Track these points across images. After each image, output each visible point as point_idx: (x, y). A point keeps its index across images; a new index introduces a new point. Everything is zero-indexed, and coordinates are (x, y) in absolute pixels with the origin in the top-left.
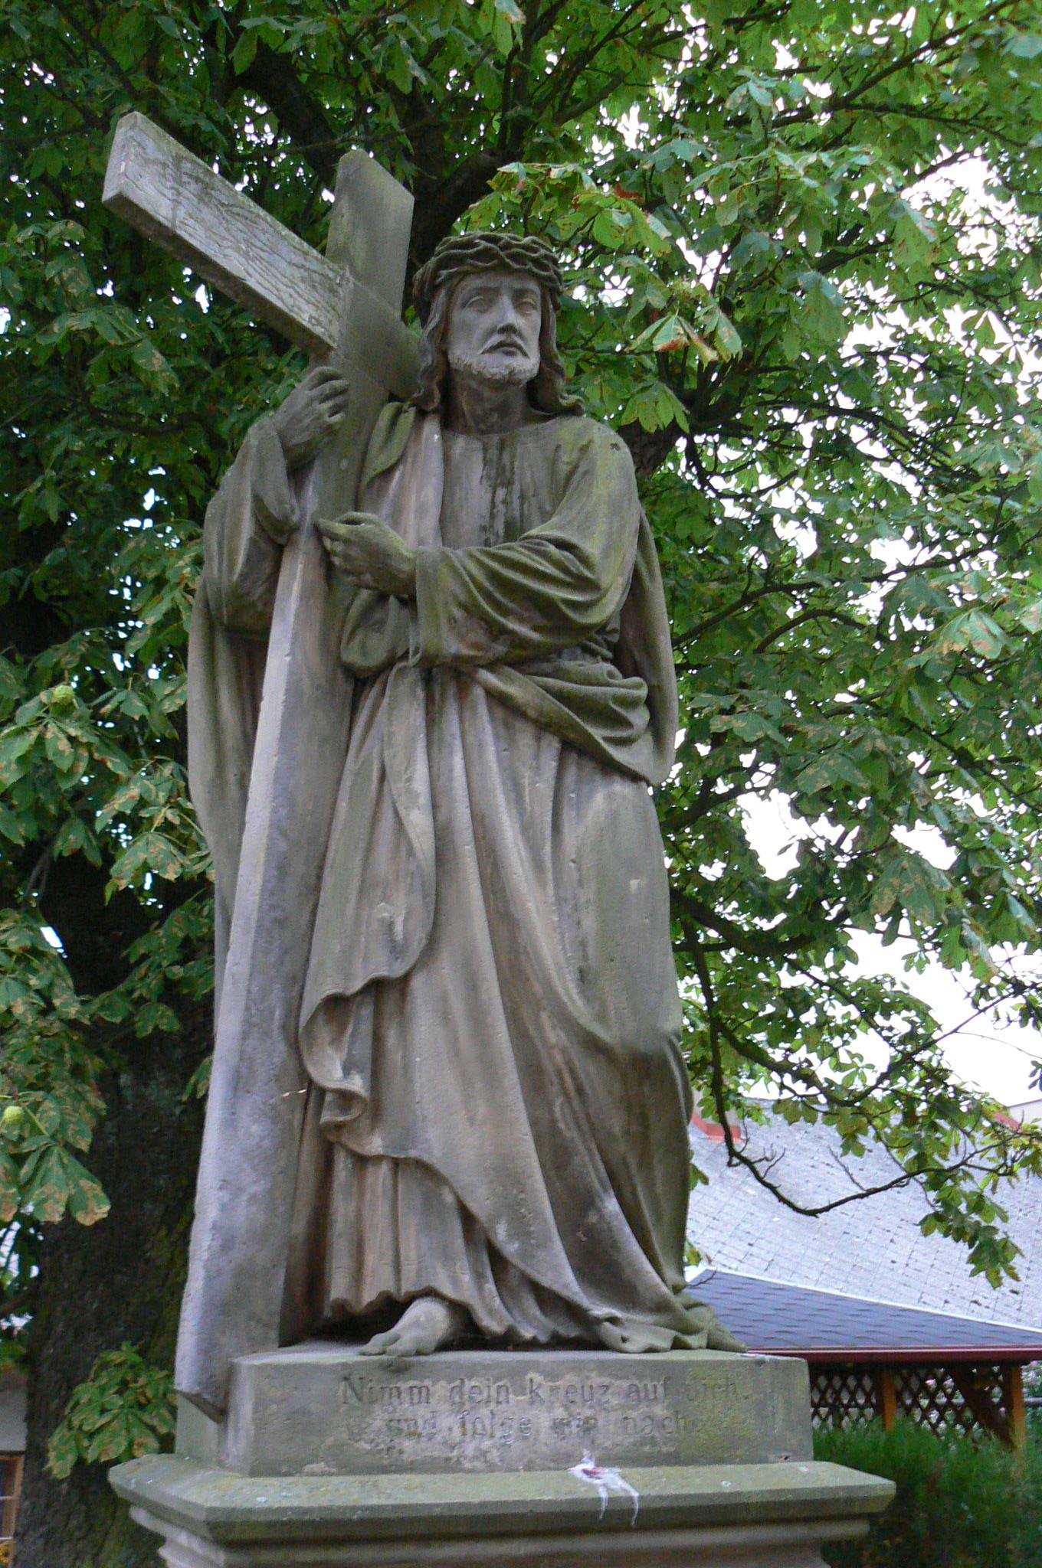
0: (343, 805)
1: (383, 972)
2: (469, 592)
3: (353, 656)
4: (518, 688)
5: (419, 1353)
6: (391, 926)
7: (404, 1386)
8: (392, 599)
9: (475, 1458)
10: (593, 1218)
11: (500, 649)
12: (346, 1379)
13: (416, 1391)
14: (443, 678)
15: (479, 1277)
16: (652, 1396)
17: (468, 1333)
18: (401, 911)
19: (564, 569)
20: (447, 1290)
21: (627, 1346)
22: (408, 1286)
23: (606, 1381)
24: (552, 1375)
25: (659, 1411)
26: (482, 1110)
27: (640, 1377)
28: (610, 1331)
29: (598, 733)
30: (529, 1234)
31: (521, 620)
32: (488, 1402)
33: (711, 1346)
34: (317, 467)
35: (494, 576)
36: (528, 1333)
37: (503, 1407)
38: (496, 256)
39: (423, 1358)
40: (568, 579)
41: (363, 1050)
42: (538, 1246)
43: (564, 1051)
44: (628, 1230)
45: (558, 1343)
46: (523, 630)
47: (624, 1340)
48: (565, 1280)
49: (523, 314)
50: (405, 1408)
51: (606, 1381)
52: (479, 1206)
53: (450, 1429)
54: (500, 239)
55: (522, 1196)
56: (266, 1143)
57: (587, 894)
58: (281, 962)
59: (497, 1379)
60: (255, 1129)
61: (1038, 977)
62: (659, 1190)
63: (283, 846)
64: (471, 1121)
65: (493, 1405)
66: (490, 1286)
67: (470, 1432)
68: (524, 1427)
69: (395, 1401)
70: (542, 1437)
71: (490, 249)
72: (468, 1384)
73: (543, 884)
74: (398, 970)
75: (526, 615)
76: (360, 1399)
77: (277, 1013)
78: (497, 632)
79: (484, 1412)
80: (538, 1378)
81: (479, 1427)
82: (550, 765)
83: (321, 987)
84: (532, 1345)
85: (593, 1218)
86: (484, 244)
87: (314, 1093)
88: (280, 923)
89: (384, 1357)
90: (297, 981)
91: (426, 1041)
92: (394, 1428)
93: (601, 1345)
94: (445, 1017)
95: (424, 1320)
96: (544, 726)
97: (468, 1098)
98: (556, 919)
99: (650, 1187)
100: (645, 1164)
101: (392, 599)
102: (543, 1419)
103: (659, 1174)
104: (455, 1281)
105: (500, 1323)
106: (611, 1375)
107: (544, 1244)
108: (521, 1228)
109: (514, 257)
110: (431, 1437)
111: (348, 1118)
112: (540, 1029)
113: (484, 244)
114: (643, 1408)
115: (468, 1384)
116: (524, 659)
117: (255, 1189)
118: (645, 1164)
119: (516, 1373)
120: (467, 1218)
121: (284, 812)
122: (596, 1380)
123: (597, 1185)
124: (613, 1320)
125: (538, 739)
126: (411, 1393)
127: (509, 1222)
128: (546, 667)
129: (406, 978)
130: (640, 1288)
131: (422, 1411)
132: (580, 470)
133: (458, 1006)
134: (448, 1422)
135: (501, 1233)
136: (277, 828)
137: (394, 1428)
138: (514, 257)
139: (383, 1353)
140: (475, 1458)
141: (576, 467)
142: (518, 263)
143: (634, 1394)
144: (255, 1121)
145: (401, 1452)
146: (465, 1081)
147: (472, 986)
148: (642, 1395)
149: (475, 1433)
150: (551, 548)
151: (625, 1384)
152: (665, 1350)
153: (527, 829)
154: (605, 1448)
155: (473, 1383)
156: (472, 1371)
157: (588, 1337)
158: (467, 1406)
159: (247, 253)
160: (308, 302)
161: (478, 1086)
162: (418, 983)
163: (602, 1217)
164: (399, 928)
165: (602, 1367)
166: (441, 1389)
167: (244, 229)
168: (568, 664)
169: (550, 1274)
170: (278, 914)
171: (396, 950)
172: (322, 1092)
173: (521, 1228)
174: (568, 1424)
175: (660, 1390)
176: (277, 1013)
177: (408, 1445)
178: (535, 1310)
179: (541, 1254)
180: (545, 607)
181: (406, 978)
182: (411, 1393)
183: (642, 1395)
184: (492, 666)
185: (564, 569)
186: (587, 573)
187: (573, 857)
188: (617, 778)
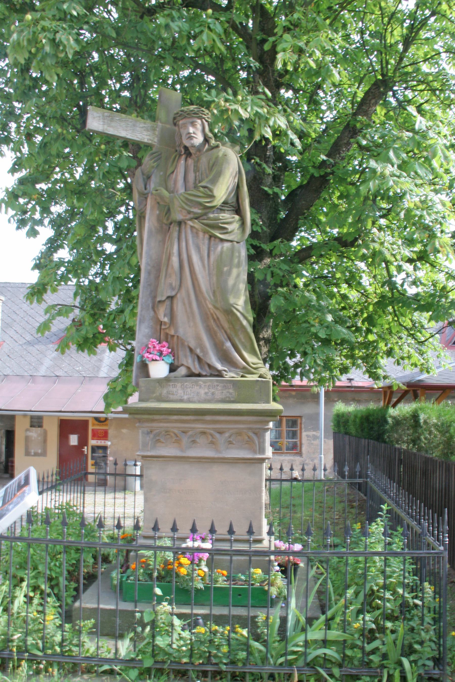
8: (36, 227)
11: (192, 216)
15: (194, 361)
17: (191, 375)
18: (174, 280)
22: (180, 363)
24: (205, 382)
25: (231, 391)
26: (192, 324)
28: (225, 373)
33: (260, 377)
35: (187, 199)
36: (204, 373)
45: (211, 375)
50: (171, 389)
52: (192, 345)
57: (215, 272)
60: (147, 331)
61: (451, 276)
63: (149, 268)
68: (198, 394)
78: (189, 212)
79: (189, 390)
80: (201, 383)
82: (206, 242)
84: (206, 376)
88: (150, 285)
90: (155, 297)
91: (179, 308)
92: (168, 393)
93: (221, 376)
94: (184, 304)
99: (240, 340)
100: (237, 335)
101: (36, 227)
102: (202, 392)
104: (187, 362)
109: (188, 114)
112: (206, 305)
114: (227, 390)
119: (196, 382)
122: (216, 384)
124: (225, 371)
128: (205, 217)
129: (176, 294)
131: (175, 390)
133: (186, 301)
134: (180, 392)
135: (198, 351)
136: (147, 264)
137: (168, 393)
138: (188, 114)
143: (225, 387)
150: (201, 189)
153: (201, 259)
162: (179, 295)
163: (336, 401)
164: (174, 284)
166: (179, 385)
178: (207, 368)
180: (200, 204)
184: (191, 219)
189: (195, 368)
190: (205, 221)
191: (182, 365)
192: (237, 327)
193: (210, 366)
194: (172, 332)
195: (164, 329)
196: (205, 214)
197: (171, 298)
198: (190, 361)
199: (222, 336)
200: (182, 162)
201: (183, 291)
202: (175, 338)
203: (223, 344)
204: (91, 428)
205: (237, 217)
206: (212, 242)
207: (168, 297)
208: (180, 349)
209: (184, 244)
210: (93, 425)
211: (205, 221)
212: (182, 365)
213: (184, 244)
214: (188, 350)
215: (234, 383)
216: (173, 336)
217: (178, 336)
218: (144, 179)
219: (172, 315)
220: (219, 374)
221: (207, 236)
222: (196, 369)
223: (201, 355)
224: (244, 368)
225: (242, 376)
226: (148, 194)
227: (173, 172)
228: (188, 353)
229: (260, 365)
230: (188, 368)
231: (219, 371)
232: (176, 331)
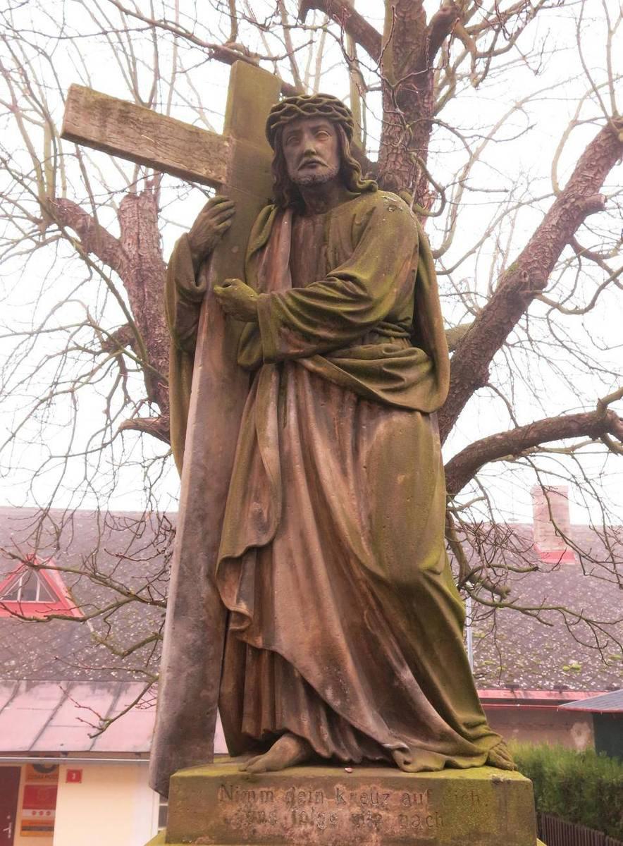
0: (239, 447)
1: (254, 543)
2: (284, 312)
3: (242, 360)
4: (324, 367)
5: (269, 770)
6: (261, 514)
7: (258, 791)
9: (302, 837)
10: (396, 684)
12: (222, 786)
13: (265, 794)
14: (285, 365)
15: (317, 723)
16: (419, 801)
17: (310, 758)
18: (262, 506)
19: (343, 291)
20: (295, 729)
21: (409, 767)
23: (388, 791)
24: (351, 784)
27: (411, 789)
28: (400, 756)
29: (376, 388)
30: (345, 695)
31: (324, 327)
32: (310, 802)
33: (489, 763)
34: (215, 254)
36: (346, 758)
37: (318, 806)
38: (296, 111)
39: (271, 774)
40: (349, 298)
41: (249, 587)
42: (351, 702)
43: (366, 582)
44: (419, 690)
46: (322, 333)
47: (406, 763)
48: (371, 722)
49: (321, 141)
51: (388, 791)
53: (286, 818)
54: (297, 99)
55: (339, 672)
56: (199, 642)
58: (204, 539)
59: (316, 788)
60: (189, 635)
62: (444, 664)
64: (307, 628)
65: (313, 804)
66: (324, 729)
67: (298, 821)
69: (252, 800)
70: (345, 825)
71: (292, 107)
72: (297, 791)
73: (346, 482)
74: (264, 540)
75: (325, 324)
76: (231, 798)
77: (202, 569)
78: (308, 337)
81: (304, 818)
82: (350, 411)
83: (224, 553)
84: (351, 764)
85: (396, 684)
86: (288, 105)
87: (227, 614)
89: (246, 773)
90: (215, 548)
91: (282, 578)
93: (393, 765)
94: (292, 567)
95: (285, 747)
96: (344, 388)
97: (304, 615)
98: (355, 503)
102: (345, 813)
103: (440, 653)
104: (300, 724)
105: (328, 750)
106: (391, 787)
107: (355, 700)
108: (340, 691)
110: (273, 823)
111: (242, 627)
113: (288, 105)
115: (297, 791)
116: (328, 350)
117: (191, 670)
118: (427, 647)
120: (309, 689)
121: (201, 455)
123: (395, 663)
124: (402, 750)
125: (343, 396)
126: (267, 795)
127: (334, 688)
129: (271, 544)
130: (432, 727)
132: (368, 227)
133: (298, 559)
134: (285, 812)
135: (329, 694)
138: (308, 109)
139: (245, 770)
140: (302, 837)
141: (366, 224)
142: (309, 111)
144: (190, 631)
145: (254, 831)
146: (302, 602)
147: (306, 551)
148: (412, 800)
149: (301, 821)
150: (338, 282)
151: (400, 793)
152: (437, 770)
154: (386, 835)
155: (300, 790)
156: (301, 782)
157: (387, 759)
158: (296, 804)
159: (156, 144)
160: (202, 161)
161: (311, 606)
162: (278, 546)
163: (401, 683)
165: (386, 782)
166: (280, 794)
167: (151, 130)
168: (360, 348)
169: (358, 721)
170: (201, 512)
171: (264, 528)
172: (229, 612)
173: (340, 691)
174: (362, 818)
175: (425, 798)
176: (202, 569)
177: (259, 827)
178: (354, 743)
179: (353, 708)
180: (335, 317)
181: (271, 544)
182: (267, 795)
183: (412, 800)
185: (343, 291)
186: (361, 292)
187: (364, 465)
188: (395, 413)
189: (323, 744)
190: (346, 361)
191: (286, 732)
192: (432, 631)
193: (362, 738)
194: (259, 642)
195: (235, 632)
196: (347, 344)
197: (261, 554)
198: (306, 720)
199: (391, 651)
200: (286, 223)
201: (292, 537)
202: (266, 656)
203: (392, 674)
204: (23, 783)
205: (420, 353)
206: (365, 412)
207: (250, 550)
208: (279, 687)
209: (292, 416)
210: (29, 777)
211: (346, 361)
212: (286, 732)
213: (292, 416)
214: (302, 691)
215: (435, 790)
216: (258, 652)
217: (274, 654)
218: (194, 261)
219: (262, 598)
220: (387, 759)
221: (350, 397)
222: (325, 744)
223: (336, 704)
224: (444, 737)
225: (449, 766)
226: (203, 294)
227: (263, 248)
228: (303, 700)
229: (482, 730)
230: (302, 741)
231: (388, 752)
232: (270, 638)
